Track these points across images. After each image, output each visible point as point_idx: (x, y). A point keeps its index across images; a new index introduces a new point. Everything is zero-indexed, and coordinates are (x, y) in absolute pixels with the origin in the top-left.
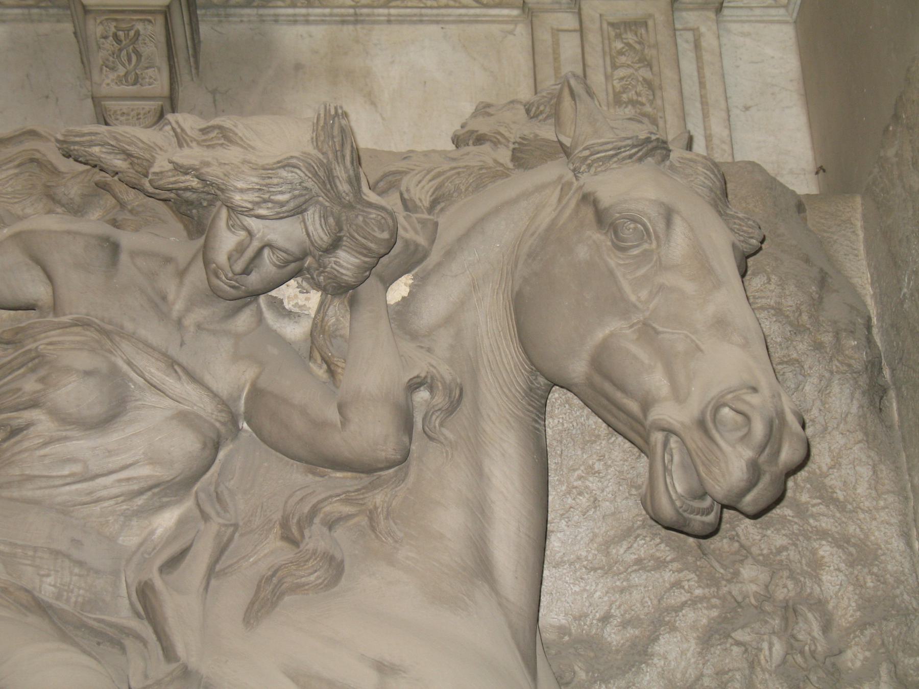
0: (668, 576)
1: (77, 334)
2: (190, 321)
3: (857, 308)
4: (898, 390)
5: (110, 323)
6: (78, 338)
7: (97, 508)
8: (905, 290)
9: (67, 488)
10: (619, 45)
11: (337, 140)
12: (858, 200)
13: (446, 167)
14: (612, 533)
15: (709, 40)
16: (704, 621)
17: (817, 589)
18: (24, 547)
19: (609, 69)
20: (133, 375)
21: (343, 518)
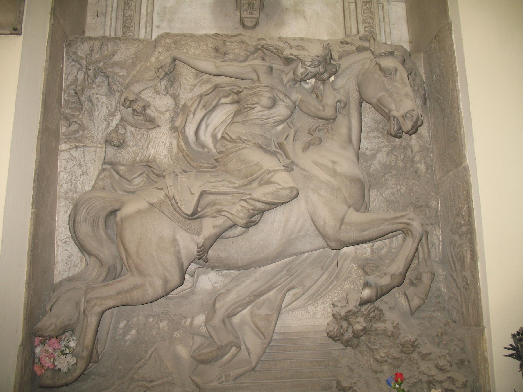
0: (380, 140)
1: (265, 88)
2: (288, 86)
3: (422, 81)
4: (430, 100)
5: (272, 86)
6: (266, 89)
7: (267, 125)
8: (434, 78)
9: (262, 121)
10: (365, 7)
11: (328, 51)
12: (422, 53)
13: (341, 50)
14: (369, 130)
15: (386, 6)
16: (388, 150)
17: (410, 144)
18: (255, 134)
19: (363, 14)
20: (277, 98)
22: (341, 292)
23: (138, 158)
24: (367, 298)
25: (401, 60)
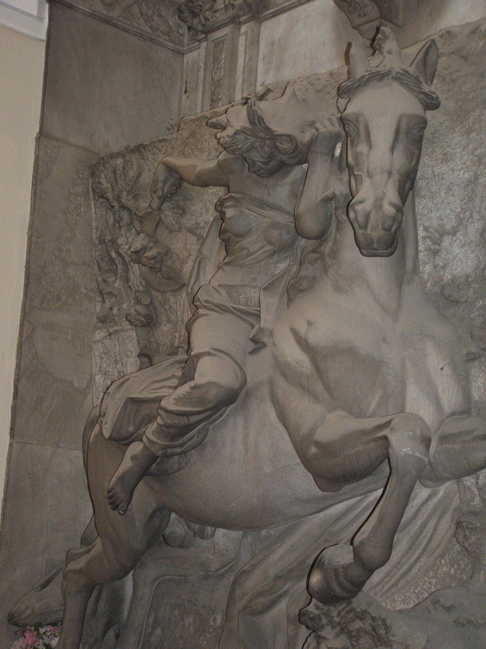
22: (433, 581)
23: (177, 340)
25: (445, 611)
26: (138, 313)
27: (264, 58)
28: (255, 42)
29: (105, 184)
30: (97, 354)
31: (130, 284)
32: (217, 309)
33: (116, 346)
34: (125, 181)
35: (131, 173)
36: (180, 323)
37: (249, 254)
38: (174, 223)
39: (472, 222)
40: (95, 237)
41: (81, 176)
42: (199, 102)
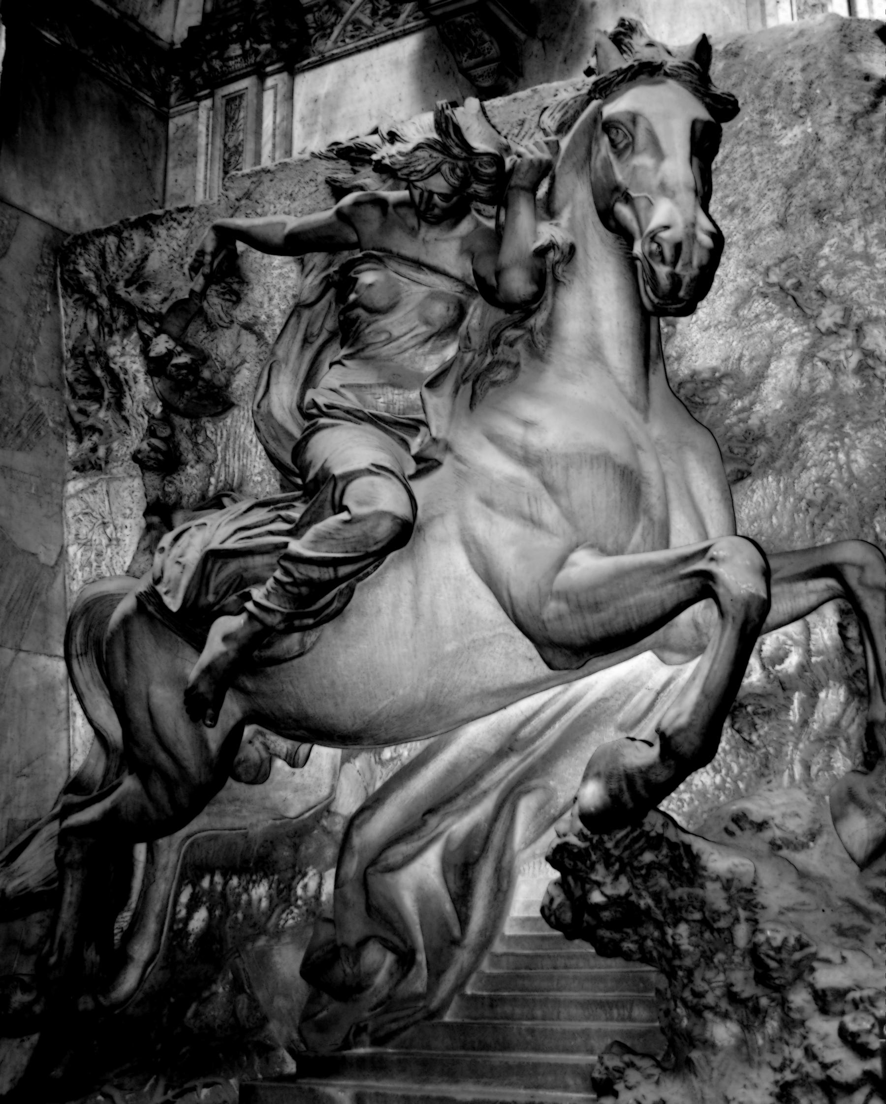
7: (407, 355)
21: (516, 340)
23: (212, 488)
24: (596, 808)
26: (154, 448)
27: (303, 119)
28: (290, 97)
29: (85, 273)
30: (70, 514)
31: (125, 413)
32: (349, 416)
33: (103, 502)
34: (120, 266)
35: (131, 256)
36: (219, 463)
37: (391, 340)
38: (222, 315)
39: (722, 295)
40: (64, 349)
41: (46, 261)
42: (201, 176)
